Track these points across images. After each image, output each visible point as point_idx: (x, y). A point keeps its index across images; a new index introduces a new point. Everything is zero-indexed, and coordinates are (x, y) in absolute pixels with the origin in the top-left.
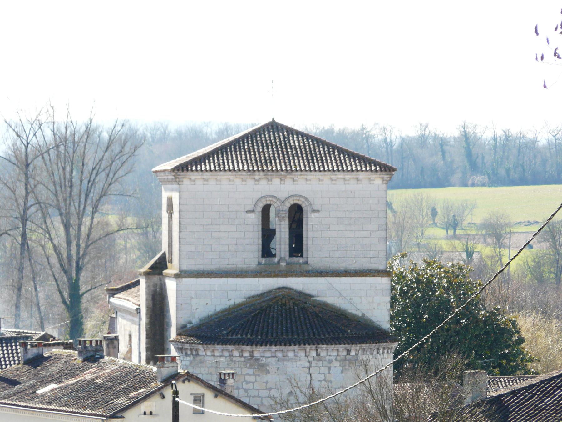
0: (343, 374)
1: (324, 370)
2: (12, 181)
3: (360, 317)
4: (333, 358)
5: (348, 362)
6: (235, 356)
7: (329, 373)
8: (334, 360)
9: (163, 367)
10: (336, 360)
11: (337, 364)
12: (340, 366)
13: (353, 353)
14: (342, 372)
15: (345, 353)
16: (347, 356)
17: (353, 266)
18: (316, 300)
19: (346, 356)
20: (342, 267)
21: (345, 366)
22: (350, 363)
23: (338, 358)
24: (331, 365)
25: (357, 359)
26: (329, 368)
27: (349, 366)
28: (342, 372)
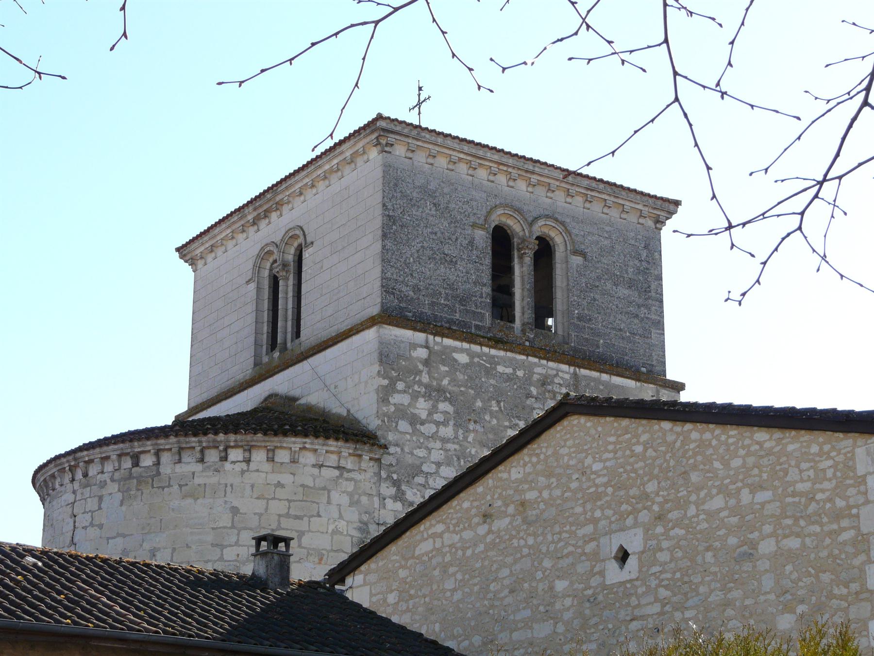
0: (124, 508)
1: (92, 504)
2: (534, 409)
3: (345, 418)
4: (106, 477)
5: (135, 481)
6: (435, 542)
7: (100, 508)
8: (108, 481)
9: (688, 600)
10: (112, 480)
11: (113, 487)
12: (119, 490)
13: (147, 461)
14: (122, 504)
15: (127, 463)
16: (134, 470)
17: (345, 323)
18: (300, 404)
19: (131, 469)
20: (332, 332)
21: (129, 489)
22: (139, 483)
23: (117, 475)
24: (104, 492)
25: (158, 473)
26: (101, 498)
27: (138, 490)
28: (122, 504)
